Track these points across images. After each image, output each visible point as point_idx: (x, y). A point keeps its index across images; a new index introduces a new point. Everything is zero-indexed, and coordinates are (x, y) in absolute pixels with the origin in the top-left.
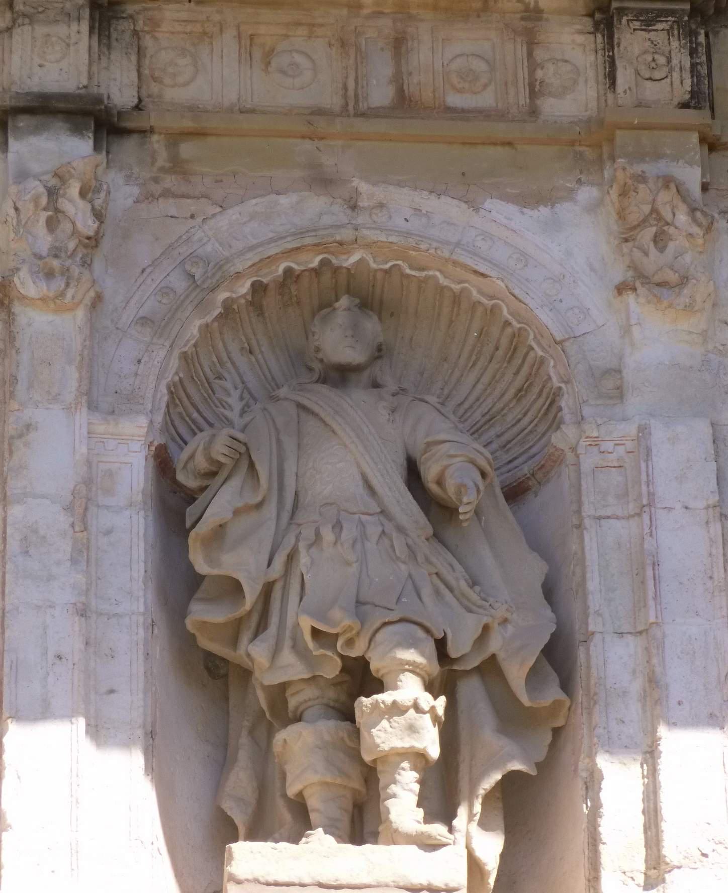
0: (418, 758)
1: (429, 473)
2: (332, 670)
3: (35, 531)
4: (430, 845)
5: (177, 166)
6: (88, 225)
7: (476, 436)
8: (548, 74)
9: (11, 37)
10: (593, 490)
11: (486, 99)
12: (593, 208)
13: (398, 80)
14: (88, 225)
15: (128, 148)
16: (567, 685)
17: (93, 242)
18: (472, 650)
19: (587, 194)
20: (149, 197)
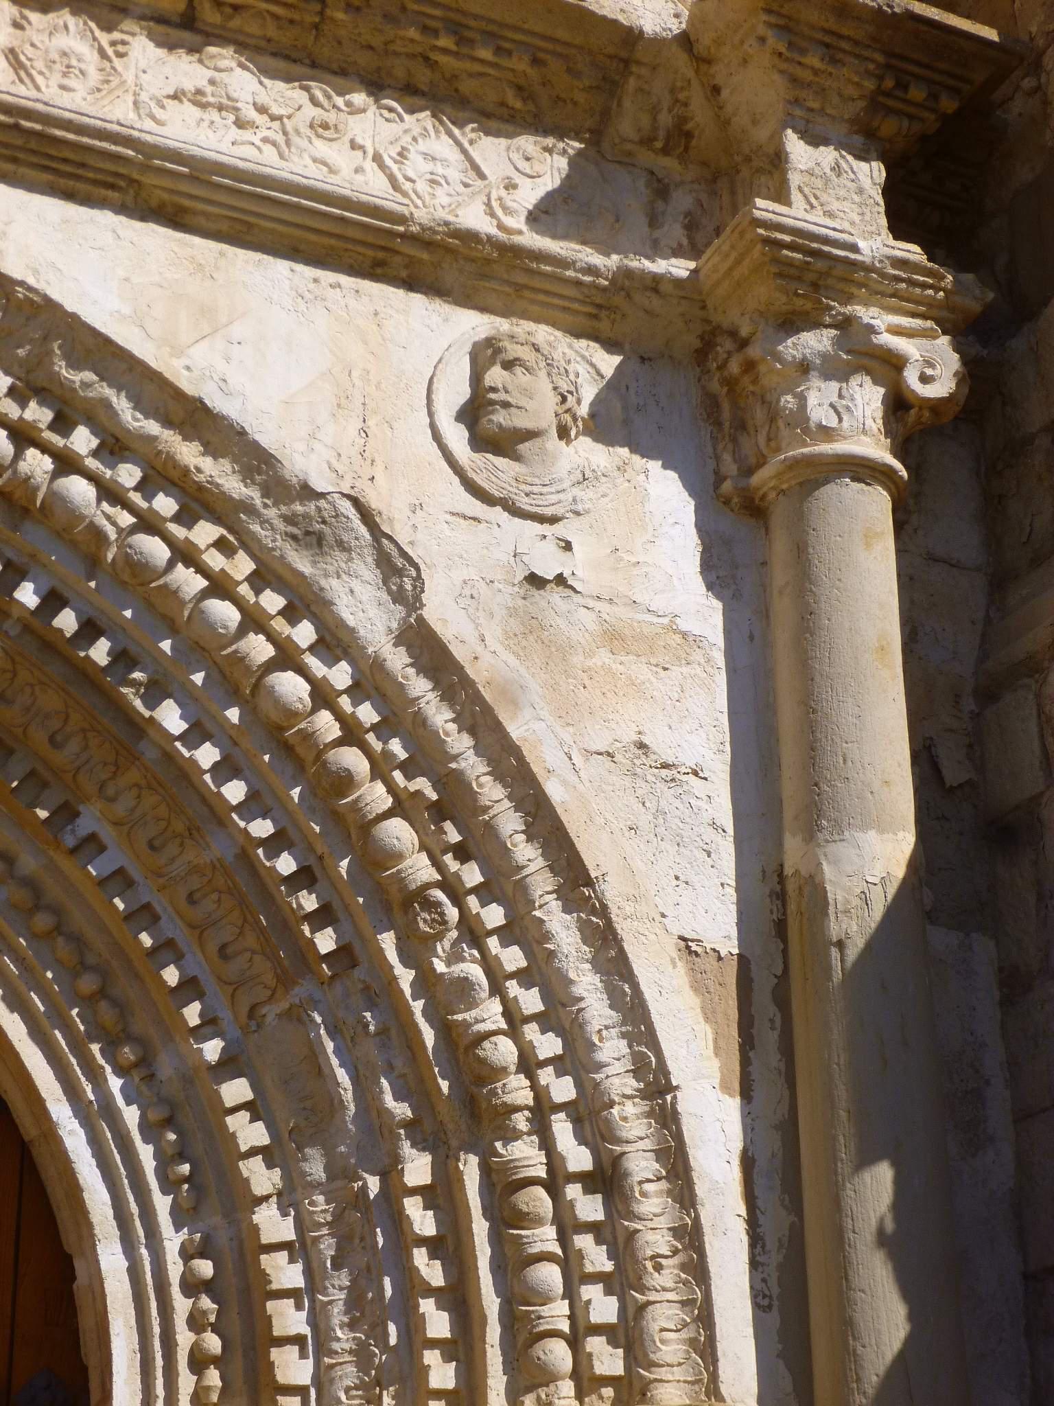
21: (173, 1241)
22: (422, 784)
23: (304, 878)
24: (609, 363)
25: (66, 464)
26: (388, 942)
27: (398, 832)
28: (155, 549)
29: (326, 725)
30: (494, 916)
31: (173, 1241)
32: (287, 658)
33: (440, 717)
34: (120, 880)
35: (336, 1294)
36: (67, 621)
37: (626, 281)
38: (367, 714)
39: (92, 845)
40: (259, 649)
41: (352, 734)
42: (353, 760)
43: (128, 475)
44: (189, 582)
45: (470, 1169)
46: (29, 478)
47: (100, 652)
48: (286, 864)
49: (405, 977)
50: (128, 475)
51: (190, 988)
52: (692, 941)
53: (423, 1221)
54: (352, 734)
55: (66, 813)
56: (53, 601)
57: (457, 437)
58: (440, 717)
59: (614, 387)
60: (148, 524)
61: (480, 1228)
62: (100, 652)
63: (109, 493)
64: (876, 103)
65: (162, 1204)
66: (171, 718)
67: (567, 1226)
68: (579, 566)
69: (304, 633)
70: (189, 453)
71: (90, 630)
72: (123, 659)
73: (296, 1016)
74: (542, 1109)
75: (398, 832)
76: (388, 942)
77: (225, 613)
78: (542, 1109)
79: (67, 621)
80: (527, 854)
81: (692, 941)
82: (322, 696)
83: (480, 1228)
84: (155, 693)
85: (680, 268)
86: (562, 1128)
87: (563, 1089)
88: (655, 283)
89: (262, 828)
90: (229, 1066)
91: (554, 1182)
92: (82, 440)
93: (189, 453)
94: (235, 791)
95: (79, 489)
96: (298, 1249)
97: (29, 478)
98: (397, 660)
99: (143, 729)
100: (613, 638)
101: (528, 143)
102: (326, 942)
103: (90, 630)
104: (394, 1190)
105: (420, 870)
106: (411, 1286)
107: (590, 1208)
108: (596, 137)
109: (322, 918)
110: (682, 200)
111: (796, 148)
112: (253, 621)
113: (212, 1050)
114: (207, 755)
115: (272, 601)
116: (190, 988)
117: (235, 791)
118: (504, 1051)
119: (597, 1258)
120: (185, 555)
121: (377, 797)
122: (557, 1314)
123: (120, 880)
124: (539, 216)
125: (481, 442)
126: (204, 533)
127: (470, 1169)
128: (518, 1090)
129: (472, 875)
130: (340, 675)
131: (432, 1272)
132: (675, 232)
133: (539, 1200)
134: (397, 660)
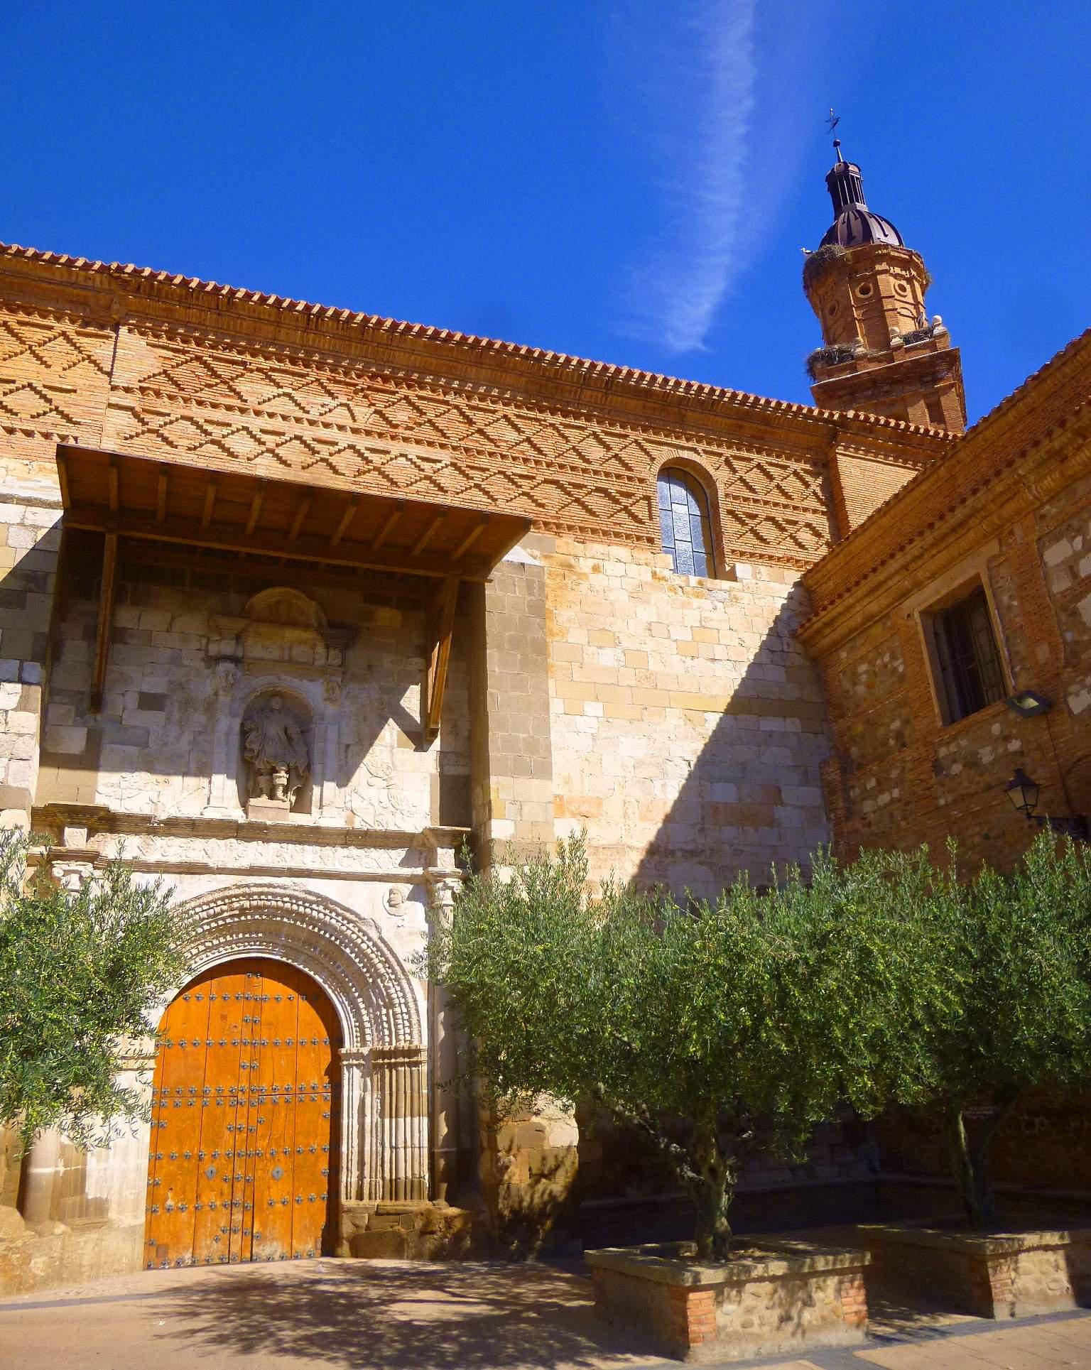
0: (283, 785)
1: (289, 732)
2: (269, 767)
3: (842, 717)
4: (284, 801)
5: (249, 670)
6: (232, 681)
7: (416, 1194)
8: (317, 656)
9: (739, 1292)
10: (1021, 404)
11: (305, 660)
12: (322, 683)
13: (290, 655)
14: (232, 681)
15: (240, 666)
16: (309, 771)
17: (232, 685)
18: (124, 1230)
19: (321, 680)
20: (244, 675)
21: (353, 1020)
22: (383, 959)
23: (367, 972)
24: (411, 887)
25: (331, 918)
26: (379, 980)
27: (380, 966)
28: (344, 928)
29: (369, 951)
30: (393, 977)
31: (353, 1020)
32: (363, 942)
33: (385, 950)
34: (343, 972)
35: (374, 1028)
36: (333, 938)
37: (413, 876)
38: (375, 949)
39: (339, 967)
40: (359, 941)
41: (373, 952)
42: (373, 956)
43: (340, 918)
44: (349, 932)
45: (391, 1011)
46: (457, 754)
47: (338, 942)
48: (365, 970)
49: (382, 985)
50: (340, 918)
51: (353, 986)
52: (961, 396)
53: (385, 1018)
54: (373, 952)
55: (335, 963)
56: (331, 936)
57: (387, 905)
58: (385, 950)
59: (412, 891)
60: (343, 925)
61: (392, 1020)
62: (338, 942)
63: (338, 921)
64: (452, 841)
65: (351, 1015)
66: (348, 951)
67: (403, 1020)
68: (405, 923)
69: (365, 938)
70: (348, 915)
71: (336, 939)
72: (341, 943)
73: (368, 990)
74: (400, 1004)
75: (380, 966)
76: (379, 980)
77: (354, 936)
78: (400, 1004)
79: (333, 938)
80: (397, 968)
81: (961, 396)
82: (368, 947)
83: (392, 1020)
84: (346, 947)
85: (419, 871)
86: (403, 1006)
87: (403, 1001)
88: (417, 876)
89: (361, 965)
90: (359, 997)
91: (402, 1013)
92: (333, 915)
93: (348, 915)
94: (357, 960)
95: (333, 921)
96: (369, 1022)
97: (457, 754)
98: (379, 942)
99: (344, 952)
100: (410, 934)
101: (399, 850)
102: (371, 980)
103: (336, 939)
104: (381, 1015)
105: (382, 971)
106: (383, 1028)
107: (406, 1017)
108: (410, 847)
109: (370, 977)
110: (424, 854)
111: (439, 850)
112: (358, 937)
113: (356, 994)
114: (353, 955)
115: (361, 934)
116: (353, 986)
117: (357, 960)
118: (394, 996)
119: (407, 1024)
120: (348, 928)
121: (376, 961)
122: (401, 1032)
123: (343, 972)
124: (403, 864)
125: (391, 906)
126: (351, 926)
127: (391, 1011)
128: (396, 1001)
129: (390, 971)
130: (371, 944)
131: (386, 1025)
132: (423, 861)
133: (399, 1016)
134: (379, 942)
